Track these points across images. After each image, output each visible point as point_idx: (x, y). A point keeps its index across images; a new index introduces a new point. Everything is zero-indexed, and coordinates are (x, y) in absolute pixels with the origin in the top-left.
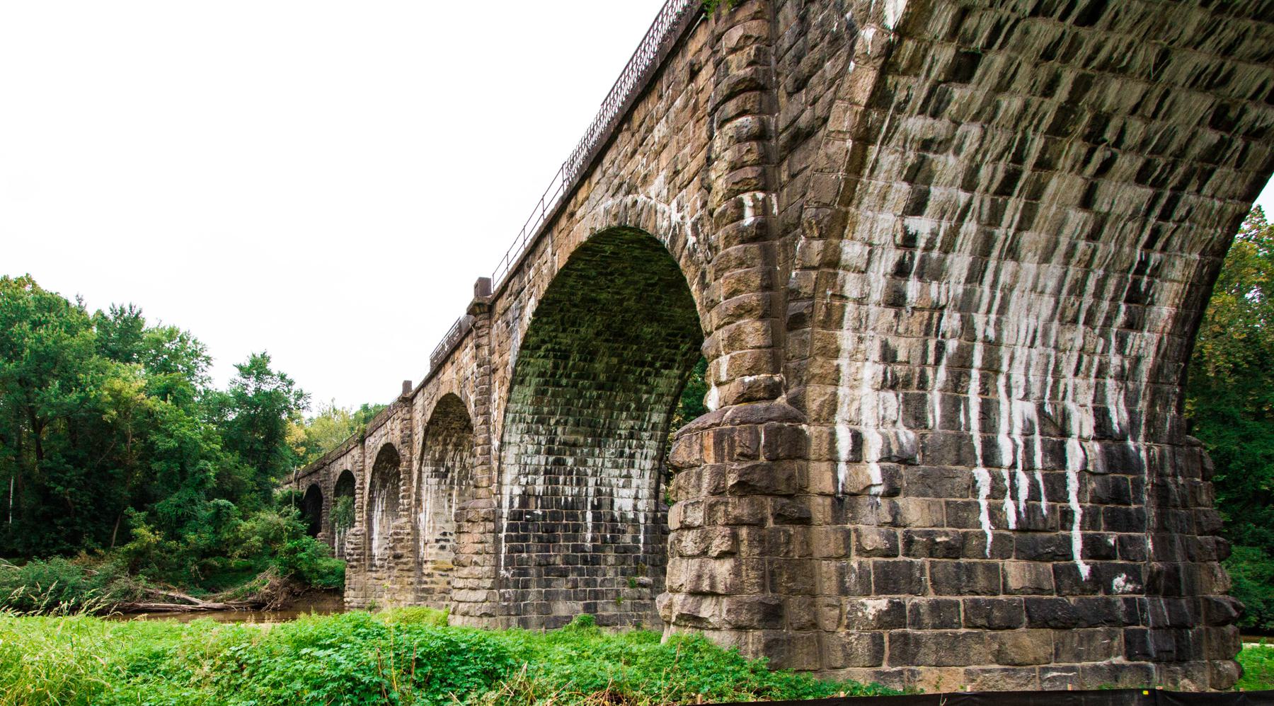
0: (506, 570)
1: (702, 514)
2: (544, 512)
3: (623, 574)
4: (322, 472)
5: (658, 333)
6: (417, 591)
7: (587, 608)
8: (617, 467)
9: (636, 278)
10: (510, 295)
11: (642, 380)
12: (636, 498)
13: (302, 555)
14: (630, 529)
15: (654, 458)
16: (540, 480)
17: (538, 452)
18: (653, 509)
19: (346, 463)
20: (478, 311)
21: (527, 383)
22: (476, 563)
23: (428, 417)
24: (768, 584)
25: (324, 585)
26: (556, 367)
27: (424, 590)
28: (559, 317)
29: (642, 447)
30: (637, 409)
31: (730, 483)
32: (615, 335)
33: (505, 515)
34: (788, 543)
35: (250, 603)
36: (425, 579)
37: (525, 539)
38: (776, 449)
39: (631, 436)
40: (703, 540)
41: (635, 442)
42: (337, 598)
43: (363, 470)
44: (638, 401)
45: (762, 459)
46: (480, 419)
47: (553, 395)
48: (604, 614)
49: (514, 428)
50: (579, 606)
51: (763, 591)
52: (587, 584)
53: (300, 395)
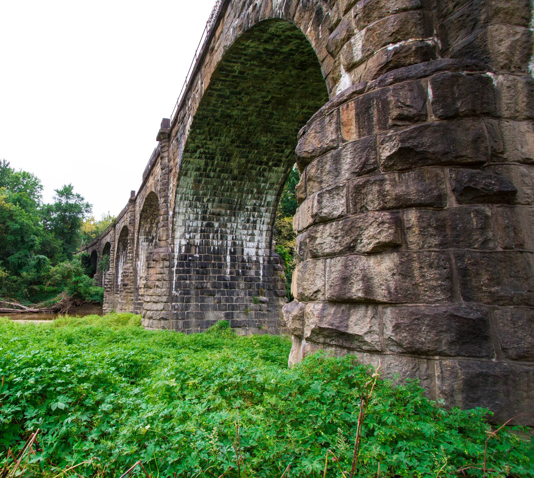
0: (176, 291)
1: (343, 201)
2: (200, 256)
3: (250, 294)
4: (98, 244)
5: (271, 142)
6: (135, 304)
7: (227, 316)
8: (245, 229)
9: (256, 97)
10: (179, 123)
11: (261, 174)
12: (258, 248)
13: (81, 284)
14: (254, 267)
15: (268, 224)
16: (198, 236)
17: (196, 219)
18: (268, 255)
19: (108, 239)
20: (162, 138)
21: (189, 175)
22: (158, 287)
23: (141, 208)
24: (458, 289)
25: (92, 301)
26: (207, 164)
27: (139, 304)
28: (207, 129)
29: (261, 217)
30: (258, 193)
31: (385, 153)
32: (243, 143)
33: (176, 257)
34: (483, 229)
35: (53, 309)
36: (140, 297)
37: (188, 272)
38: (454, 104)
39: (254, 210)
40: (347, 233)
41: (256, 213)
42: (99, 307)
43: (114, 241)
44: (258, 187)
45: (432, 119)
46: (162, 200)
47: (205, 183)
48: (238, 319)
49: (182, 203)
50: (222, 314)
51: (451, 298)
52: (227, 300)
53: (88, 206)
